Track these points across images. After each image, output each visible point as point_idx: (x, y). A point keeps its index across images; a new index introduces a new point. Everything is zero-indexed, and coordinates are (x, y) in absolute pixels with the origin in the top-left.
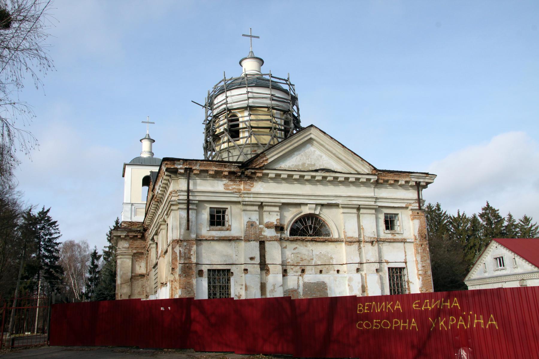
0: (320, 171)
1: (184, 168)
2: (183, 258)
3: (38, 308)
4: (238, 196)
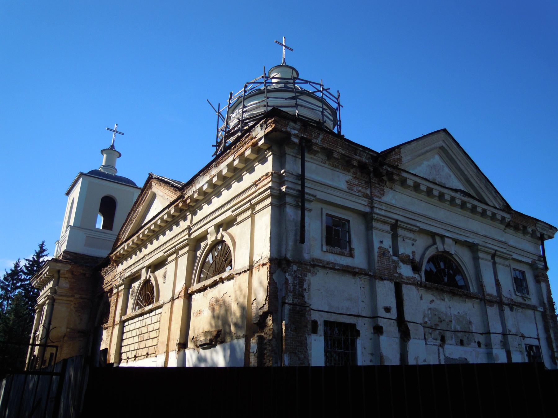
0: (459, 193)
1: (300, 136)
2: (292, 294)
3: (30, 346)
4: (366, 204)
